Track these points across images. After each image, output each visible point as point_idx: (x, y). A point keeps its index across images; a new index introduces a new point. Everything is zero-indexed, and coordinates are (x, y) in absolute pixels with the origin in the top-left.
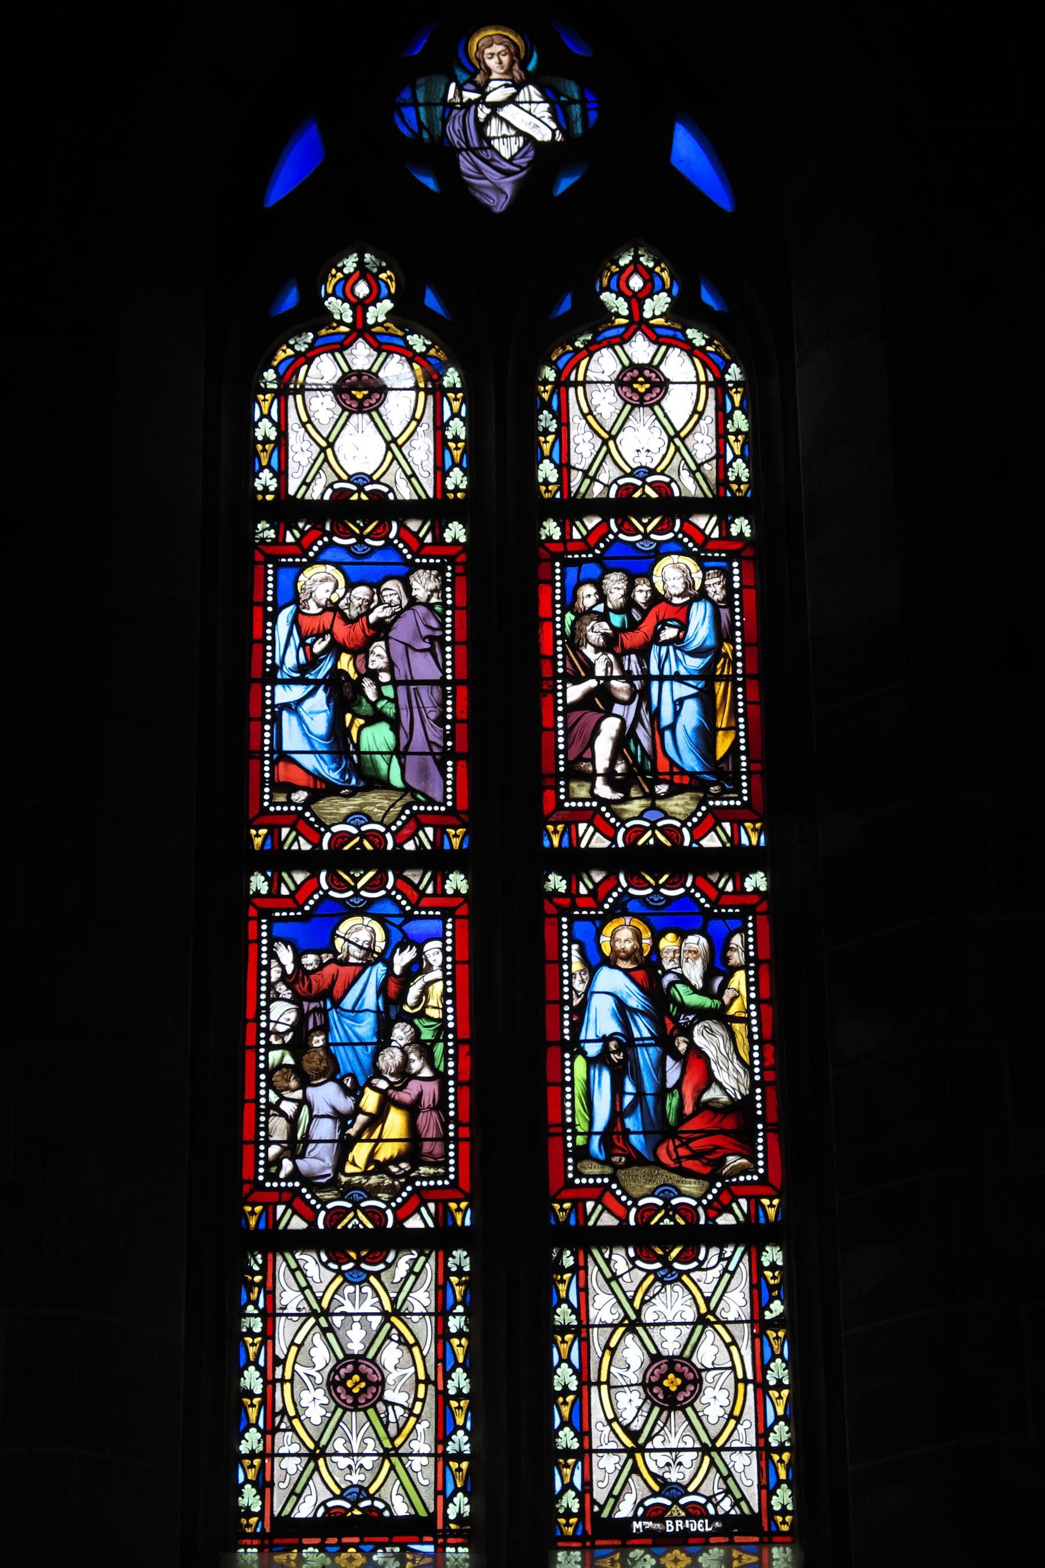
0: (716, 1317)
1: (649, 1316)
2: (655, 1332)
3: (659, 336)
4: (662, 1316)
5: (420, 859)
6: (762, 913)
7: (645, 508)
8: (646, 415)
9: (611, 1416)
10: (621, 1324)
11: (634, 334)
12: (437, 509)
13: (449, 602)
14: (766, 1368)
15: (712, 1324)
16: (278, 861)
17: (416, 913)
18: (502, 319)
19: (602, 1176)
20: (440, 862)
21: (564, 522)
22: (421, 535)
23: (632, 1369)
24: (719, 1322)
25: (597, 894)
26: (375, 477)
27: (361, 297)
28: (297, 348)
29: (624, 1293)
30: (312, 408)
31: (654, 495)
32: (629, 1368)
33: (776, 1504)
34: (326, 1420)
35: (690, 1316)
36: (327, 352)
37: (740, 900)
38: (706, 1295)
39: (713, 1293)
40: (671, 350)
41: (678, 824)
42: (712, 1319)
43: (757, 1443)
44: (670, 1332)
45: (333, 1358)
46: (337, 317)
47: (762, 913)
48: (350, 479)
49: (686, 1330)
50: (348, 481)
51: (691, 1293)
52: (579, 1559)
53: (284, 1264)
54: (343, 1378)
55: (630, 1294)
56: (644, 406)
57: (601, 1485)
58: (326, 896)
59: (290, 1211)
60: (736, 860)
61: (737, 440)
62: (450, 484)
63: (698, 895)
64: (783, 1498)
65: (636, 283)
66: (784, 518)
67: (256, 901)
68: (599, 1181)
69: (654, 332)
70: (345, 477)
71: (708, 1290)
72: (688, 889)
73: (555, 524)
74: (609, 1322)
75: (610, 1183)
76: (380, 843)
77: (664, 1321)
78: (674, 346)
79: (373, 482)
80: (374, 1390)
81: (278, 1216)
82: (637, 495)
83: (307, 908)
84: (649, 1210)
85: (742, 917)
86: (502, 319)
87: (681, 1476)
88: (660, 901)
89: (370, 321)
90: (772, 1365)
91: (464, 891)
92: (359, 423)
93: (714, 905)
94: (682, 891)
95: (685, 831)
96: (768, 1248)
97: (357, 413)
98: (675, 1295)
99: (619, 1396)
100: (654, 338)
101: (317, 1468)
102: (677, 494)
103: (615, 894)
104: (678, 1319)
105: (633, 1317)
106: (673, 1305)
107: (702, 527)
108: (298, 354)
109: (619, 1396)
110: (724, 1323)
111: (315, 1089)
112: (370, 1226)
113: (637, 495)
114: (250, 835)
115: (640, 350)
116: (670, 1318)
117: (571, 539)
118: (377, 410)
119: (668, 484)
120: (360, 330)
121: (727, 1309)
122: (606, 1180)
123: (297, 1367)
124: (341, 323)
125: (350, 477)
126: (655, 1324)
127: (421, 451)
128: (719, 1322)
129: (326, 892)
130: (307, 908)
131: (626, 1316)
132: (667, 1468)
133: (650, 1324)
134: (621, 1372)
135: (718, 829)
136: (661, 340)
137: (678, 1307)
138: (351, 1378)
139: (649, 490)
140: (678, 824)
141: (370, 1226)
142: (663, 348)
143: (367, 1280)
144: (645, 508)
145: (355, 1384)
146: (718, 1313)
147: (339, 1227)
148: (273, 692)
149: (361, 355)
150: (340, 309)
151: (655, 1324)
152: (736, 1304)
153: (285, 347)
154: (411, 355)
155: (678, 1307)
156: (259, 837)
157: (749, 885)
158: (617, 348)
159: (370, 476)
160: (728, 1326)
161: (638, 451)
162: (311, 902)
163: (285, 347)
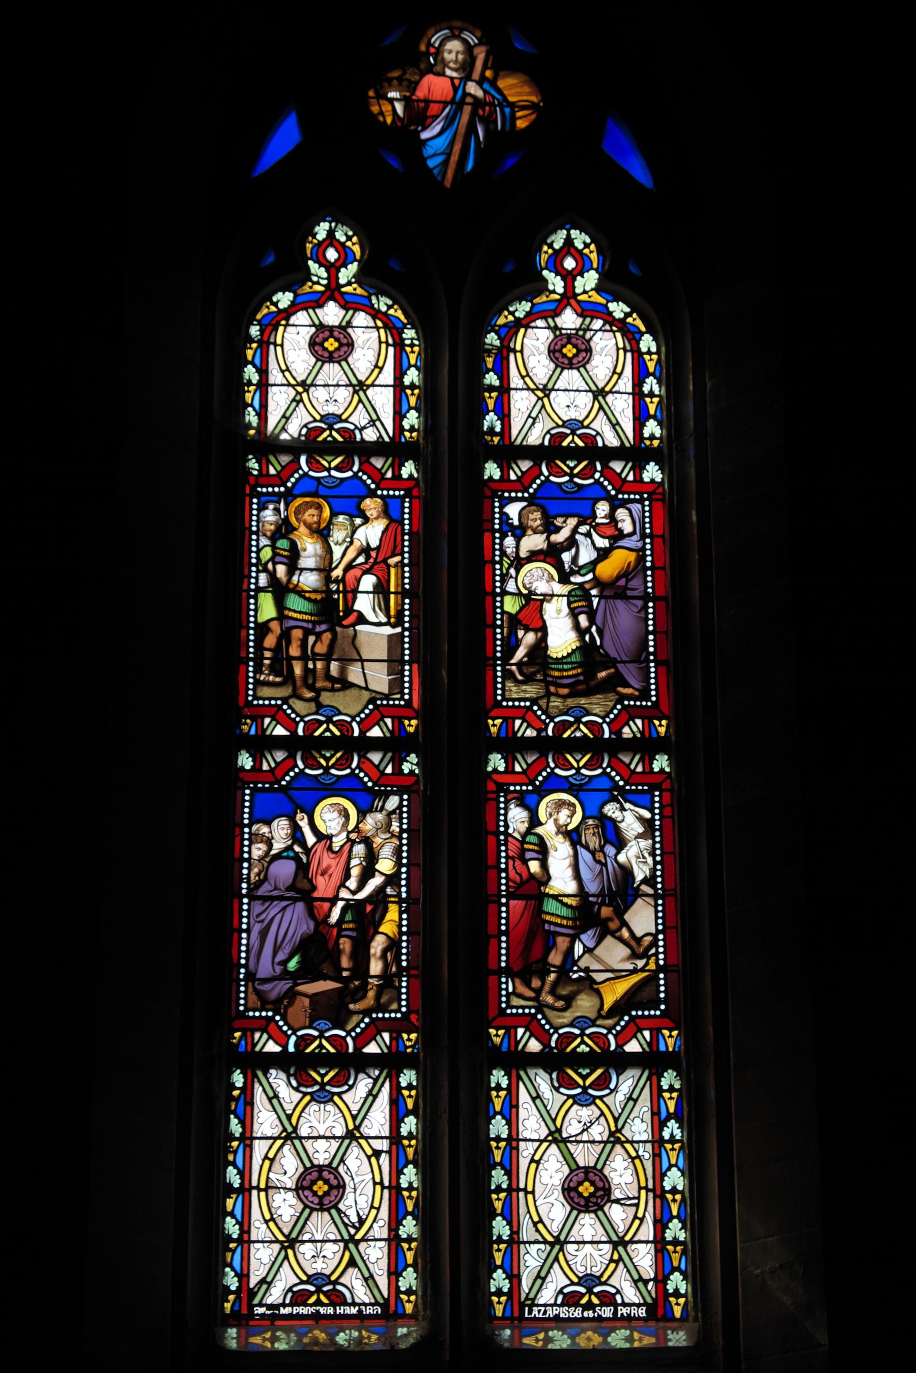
0: (360, 1133)
1: (304, 1131)
2: (308, 1144)
3: (347, 302)
4: (315, 1130)
5: (632, 745)
6: (666, 790)
7: (331, 449)
8: (576, 377)
9: (268, 1217)
10: (279, 1137)
11: (565, 308)
12: (395, 449)
13: (648, 531)
14: (400, 1172)
15: (356, 1139)
16: (261, 745)
17: (628, 787)
18: (453, 290)
19: (530, 1008)
20: (647, 746)
21: (502, 463)
22: (383, 471)
23: (289, 1174)
24: (362, 1137)
25: (529, 775)
26: (586, 423)
27: (332, 261)
28: (517, 314)
29: (284, 1111)
30: (530, 366)
31: (581, 444)
32: (285, 1173)
33: (403, 1285)
34: (295, 1218)
35: (339, 1131)
36: (302, 309)
37: (398, 780)
38: (288, 1112)
39: (359, 1111)
40: (357, 313)
41: (349, 719)
42: (358, 1135)
43: (389, 1235)
44: (321, 1144)
45: (301, 1165)
46: (551, 287)
47: (666, 790)
48: (565, 424)
49: (335, 1144)
50: (563, 426)
51: (341, 1112)
52: (235, 1335)
53: (261, 1088)
54: (313, 1186)
55: (354, 1113)
56: (333, 362)
57: (256, 1273)
58: (552, 774)
59: (528, 1034)
60: (647, 746)
61: (413, 394)
62: (646, 433)
63: (362, 775)
64: (409, 1279)
65: (332, 255)
66: (718, 467)
67: (495, 777)
68: (527, 1011)
69: (344, 299)
70: (318, 417)
71: (355, 1108)
72: (353, 770)
73: (495, 466)
74: (269, 1135)
75: (536, 1014)
76: (348, 731)
77: (317, 1135)
78: (597, 318)
79: (584, 427)
80: (591, 1174)
81: (519, 1037)
82: (565, 444)
83: (284, 783)
84: (568, 1038)
85: (650, 792)
86: (453, 290)
87: (325, 1266)
88: (582, 780)
89: (578, 290)
90: (405, 1171)
91: (667, 770)
92: (328, 369)
93: (532, 783)
94: (348, 771)
95: (354, 725)
96: (405, 1071)
97: (568, 369)
98: (327, 1114)
99: (276, 1197)
100: (343, 303)
101: (286, 1257)
102: (600, 444)
103: (544, 774)
104: (328, 1134)
105: (290, 1129)
106: (322, 1120)
107: (619, 471)
108: (517, 320)
109: (276, 1197)
110: (367, 1138)
111: (648, 931)
112: (332, 1050)
113: (565, 444)
114: (487, 724)
115: (332, 314)
116: (322, 1133)
117: (509, 480)
118: (346, 360)
119: (595, 437)
120: (333, 292)
121: (369, 1126)
122: (533, 1011)
123: (271, 1175)
124: (554, 292)
125: (564, 422)
126: (309, 1138)
127: (383, 399)
128: (362, 1137)
129: (552, 769)
130: (284, 783)
131: (285, 1130)
132: (313, 1260)
133: (305, 1138)
134: (279, 1177)
135: (381, 723)
136: (348, 306)
137: (329, 1123)
138: (325, 1184)
139: (577, 440)
140: (349, 719)
141: (332, 1050)
142: (351, 312)
143: (331, 1100)
144: (331, 449)
145: (320, 1187)
146: (362, 1130)
147: (568, 1050)
148: (502, 602)
149: (569, 320)
150: (556, 283)
151: (309, 1138)
152: (378, 1121)
153: (268, 303)
154: (373, 312)
155: (329, 1123)
156: (495, 725)
157: (406, 768)
158: (311, 311)
159: (582, 422)
160: (370, 1141)
161: (568, 406)
162: (288, 778)
163: (268, 303)
